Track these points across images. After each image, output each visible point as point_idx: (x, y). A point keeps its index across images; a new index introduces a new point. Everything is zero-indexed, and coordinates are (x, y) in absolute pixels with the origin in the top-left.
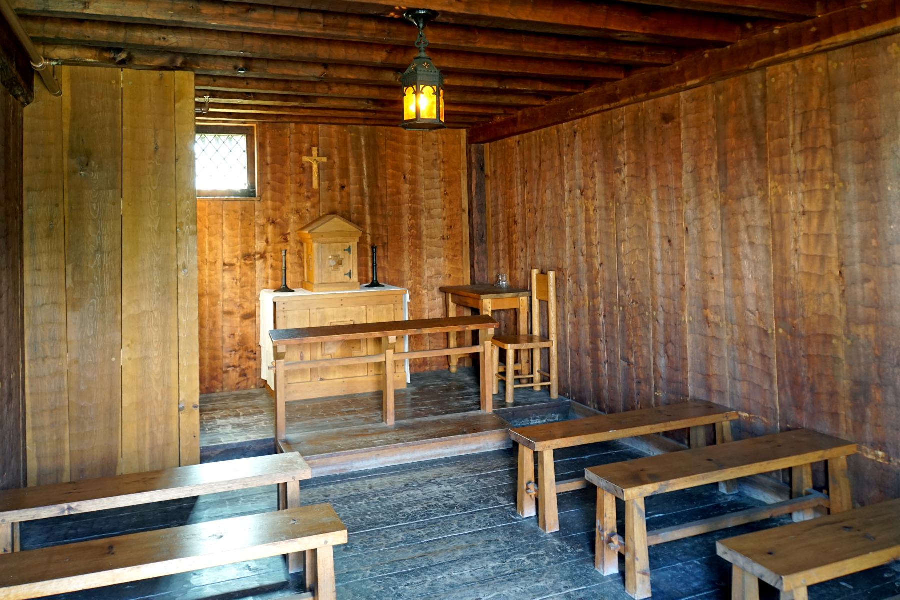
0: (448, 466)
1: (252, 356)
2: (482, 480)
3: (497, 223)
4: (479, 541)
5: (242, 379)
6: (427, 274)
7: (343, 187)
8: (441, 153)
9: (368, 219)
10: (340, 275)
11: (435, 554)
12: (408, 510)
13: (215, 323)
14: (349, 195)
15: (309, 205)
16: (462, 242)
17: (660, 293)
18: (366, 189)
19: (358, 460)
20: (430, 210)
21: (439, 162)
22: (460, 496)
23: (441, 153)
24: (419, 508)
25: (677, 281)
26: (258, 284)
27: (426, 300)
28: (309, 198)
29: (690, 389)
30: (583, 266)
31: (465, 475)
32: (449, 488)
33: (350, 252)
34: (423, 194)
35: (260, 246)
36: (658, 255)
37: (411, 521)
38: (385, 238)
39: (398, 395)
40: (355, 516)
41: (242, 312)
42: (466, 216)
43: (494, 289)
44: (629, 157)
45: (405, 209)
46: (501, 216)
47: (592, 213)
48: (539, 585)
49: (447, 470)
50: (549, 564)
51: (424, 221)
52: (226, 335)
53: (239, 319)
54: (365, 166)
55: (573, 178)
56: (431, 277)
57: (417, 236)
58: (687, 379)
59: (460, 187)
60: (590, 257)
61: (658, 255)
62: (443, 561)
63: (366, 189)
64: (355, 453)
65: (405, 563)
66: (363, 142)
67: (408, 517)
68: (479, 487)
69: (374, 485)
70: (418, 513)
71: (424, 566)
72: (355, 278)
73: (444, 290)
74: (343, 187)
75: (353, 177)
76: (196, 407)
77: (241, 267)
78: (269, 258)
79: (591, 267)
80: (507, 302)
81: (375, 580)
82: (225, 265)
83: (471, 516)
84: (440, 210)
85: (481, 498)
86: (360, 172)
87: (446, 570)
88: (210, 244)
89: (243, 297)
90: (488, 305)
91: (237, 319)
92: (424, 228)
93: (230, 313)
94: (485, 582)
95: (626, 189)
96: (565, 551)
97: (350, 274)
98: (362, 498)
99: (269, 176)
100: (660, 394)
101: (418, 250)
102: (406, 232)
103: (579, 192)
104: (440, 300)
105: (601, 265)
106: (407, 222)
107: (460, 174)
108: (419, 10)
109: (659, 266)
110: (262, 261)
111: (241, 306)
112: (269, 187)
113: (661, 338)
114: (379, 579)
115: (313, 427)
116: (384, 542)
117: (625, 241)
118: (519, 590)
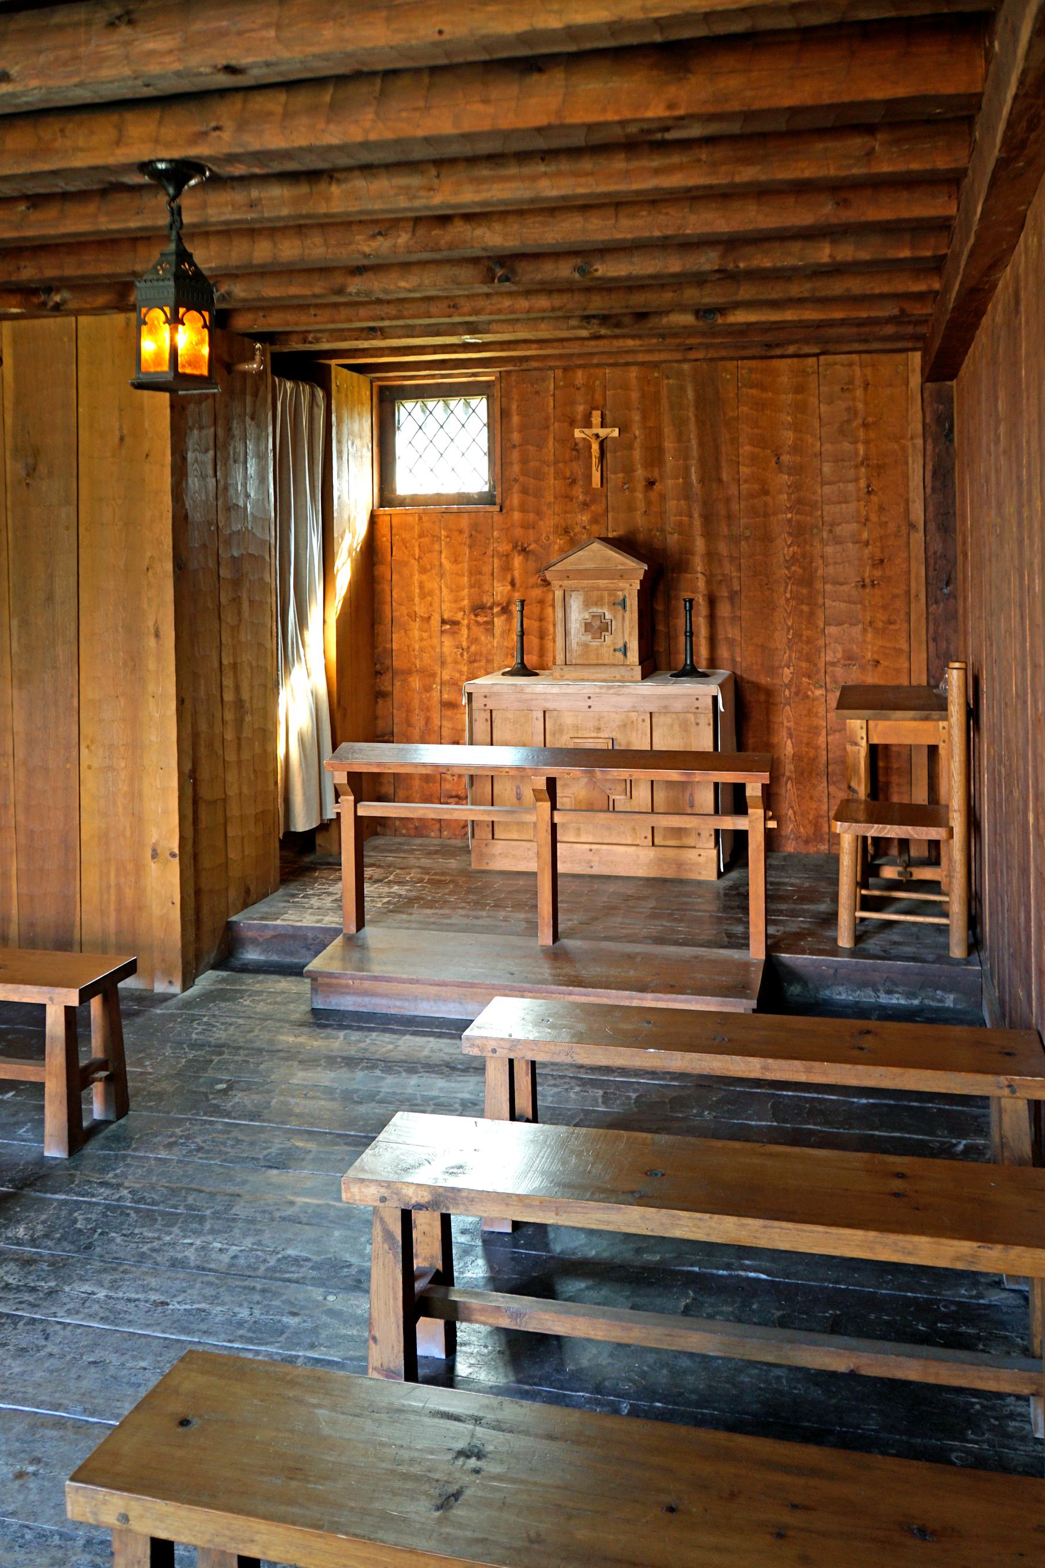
7: (651, 484)
38: (735, 583)
59: (906, 477)
74: (651, 484)
77: (469, 627)
82: (444, 622)
84: (854, 526)
88: (421, 586)
97: (625, 650)
106: (784, 547)
107: (904, 449)
110: (503, 617)
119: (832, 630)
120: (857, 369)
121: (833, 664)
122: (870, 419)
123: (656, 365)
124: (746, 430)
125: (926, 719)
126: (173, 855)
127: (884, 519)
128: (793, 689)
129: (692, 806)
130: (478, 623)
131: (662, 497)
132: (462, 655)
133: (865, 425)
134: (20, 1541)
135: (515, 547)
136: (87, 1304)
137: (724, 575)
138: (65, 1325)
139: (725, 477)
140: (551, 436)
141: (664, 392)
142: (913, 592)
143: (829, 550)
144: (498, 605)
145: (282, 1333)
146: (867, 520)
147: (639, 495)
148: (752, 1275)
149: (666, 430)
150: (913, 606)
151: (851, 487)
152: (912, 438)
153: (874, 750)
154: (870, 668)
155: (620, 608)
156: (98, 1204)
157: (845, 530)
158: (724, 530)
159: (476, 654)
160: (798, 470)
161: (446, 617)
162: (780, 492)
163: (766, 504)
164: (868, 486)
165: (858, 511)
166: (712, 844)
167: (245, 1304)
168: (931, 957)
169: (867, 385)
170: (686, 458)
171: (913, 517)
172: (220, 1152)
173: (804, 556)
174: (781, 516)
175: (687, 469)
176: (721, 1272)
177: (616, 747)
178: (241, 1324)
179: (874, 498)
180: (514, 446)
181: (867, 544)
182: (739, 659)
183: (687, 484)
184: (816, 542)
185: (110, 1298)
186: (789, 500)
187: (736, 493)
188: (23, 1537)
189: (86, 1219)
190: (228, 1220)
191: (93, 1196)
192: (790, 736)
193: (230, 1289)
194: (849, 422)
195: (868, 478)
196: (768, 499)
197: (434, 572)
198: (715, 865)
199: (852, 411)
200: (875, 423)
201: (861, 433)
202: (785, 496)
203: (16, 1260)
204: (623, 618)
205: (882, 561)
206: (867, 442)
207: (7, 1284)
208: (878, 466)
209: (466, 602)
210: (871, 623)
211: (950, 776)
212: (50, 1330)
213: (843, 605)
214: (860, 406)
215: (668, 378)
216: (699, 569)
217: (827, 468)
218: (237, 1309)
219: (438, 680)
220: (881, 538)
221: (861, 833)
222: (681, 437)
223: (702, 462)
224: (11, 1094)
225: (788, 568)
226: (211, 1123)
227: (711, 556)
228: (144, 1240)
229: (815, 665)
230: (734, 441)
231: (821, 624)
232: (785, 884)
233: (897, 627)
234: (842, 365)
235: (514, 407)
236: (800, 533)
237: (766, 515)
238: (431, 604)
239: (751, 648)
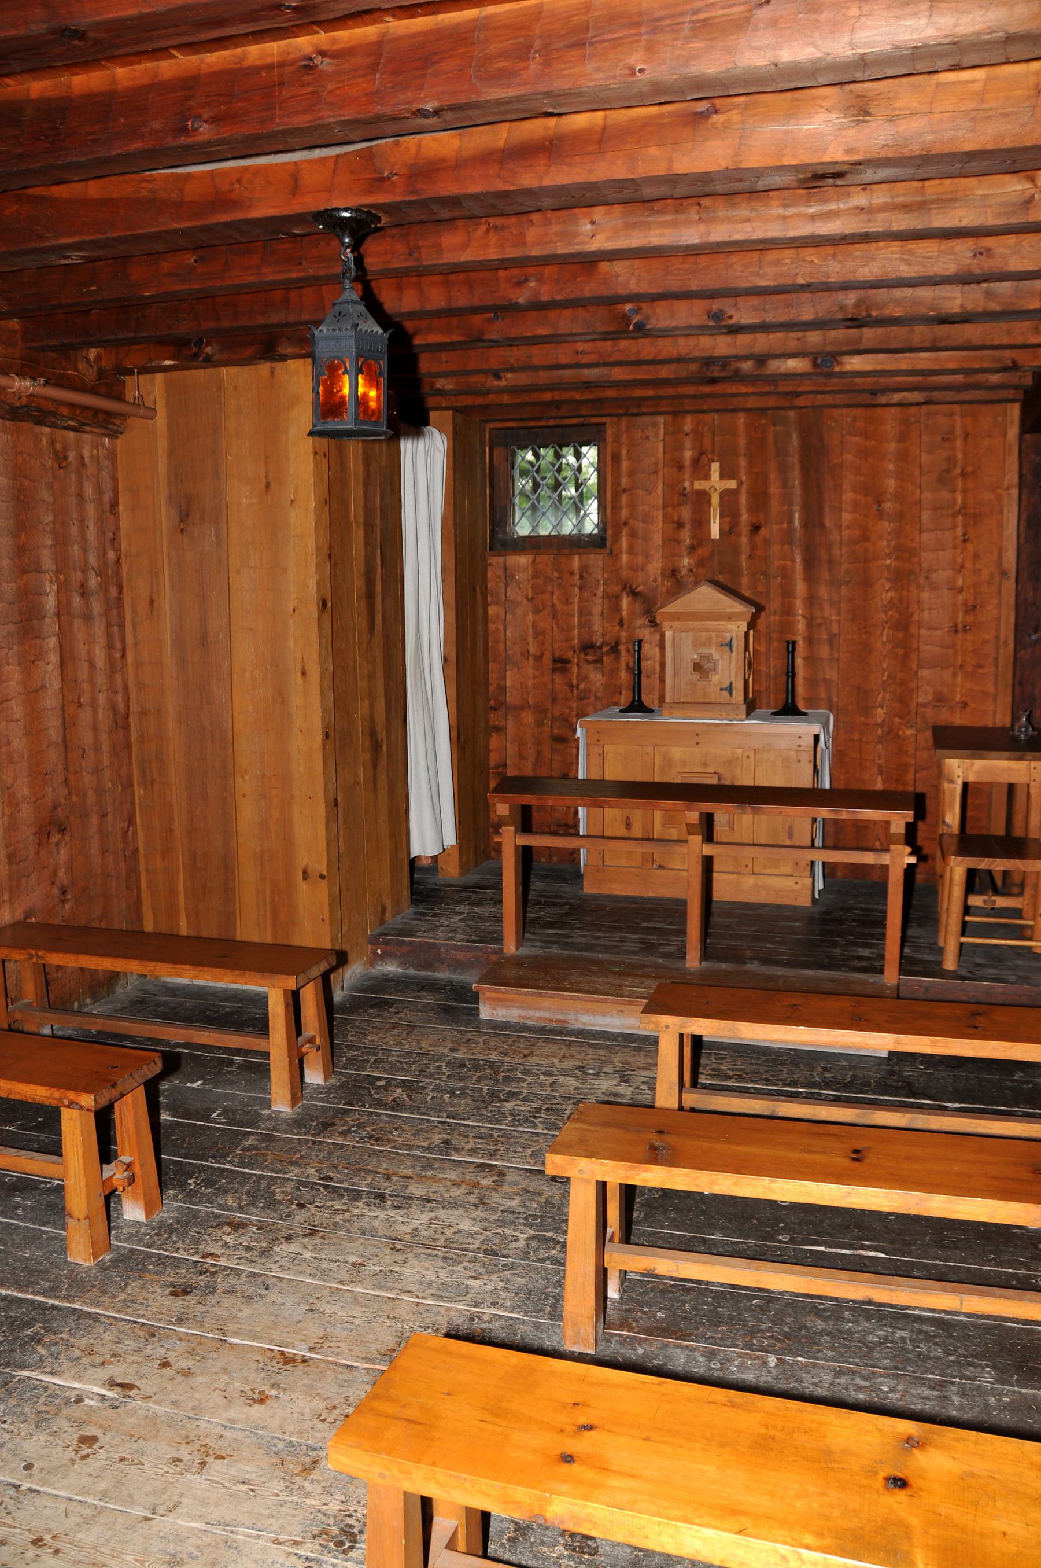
7: (756, 528)
16: (997, 638)
19: (588, 1012)
38: (835, 626)
59: (1001, 526)
64: (579, 998)
74: (756, 528)
78: (623, 653)
82: (555, 661)
84: (949, 573)
86: (787, 500)
106: (884, 593)
107: (999, 498)
108: (338, 210)
110: (613, 656)
119: (925, 673)
120: (958, 419)
121: (924, 705)
122: (969, 469)
123: (763, 410)
124: (849, 480)
125: (1020, 759)
126: (322, 877)
127: (978, 566)
128: (886, 729)
129: (790, 836)
130: (588, 662)
131: (767, 542)
133: (963, 474)
134: (274, 1449)
135: (624, 589)
136: (296, 1262)
137: (823, 618)
138: (281, 1279)
139: (828, 522)
140: (661, 481)
141: (771, 437)
142: (1002, 638)
143: (925, 595)
144: (608, 644)
145: (467, 1293)
146: (962, 567)
147: (744, 540)
148: (872, 1254)
149: (772, 476)
150: (1001, 651)
151: (948, 534)
152: (1008, 489)
153: (965, 785)
154: (958, 710)
155: (727, 649)
156: (291, 1180)
157: (942, 576)
158: (826, 575)
159: (585, 691)
160: (900, 517)
162: (880, 538)
163: (866, 550)
164: (965, 535)
165: (954, 558)
166: (808, 873)
167: (431, 1268)
168: (1012, 978)
169: (966, 435)
170: (791, 504)
171: (1005, 565)
172: (388, 1140)
173: (901, 601)
174: (880, 562)
175: (791, 515)
176: (844, 1251)
177: (723, 782)
178: (430, 1285)
179: (970, 546)
181: (961, 590)
182: (835, 699)
183: (790, 529)
184: (913, 588)
185: (316, 1258)
186: (888, 546)
187: (838, 537)
188: (275, 1446)
189: (283, 1192)
190: (405, 1198)
191: (285, 1173)
192: (881, 773)
193: (417, 1256)
194: (948, 471)
195: (964, 526)
196: (869, 545)
197: (546, 612)
198: (809, 892)
199: (951, 461)
200: (974, 473)
201: (960, 483)
202: (885, 543)
203: (229, 1224)
204: (730, 658)
205: (974, 607)
206: (964, 491)
207: (226, 1243)
208: (975, 515)
210: (961, 666)
212: (268, 1282)
213: (936, 649)
214: (959, 455)
215: (774, 425)
216: (800, 612)
217: (926, 516)
218: (424, 1272)
219: (549, 715)
220: (975, 584)
221: (972, 866)
222: (785, 484)
223: (806, 508)
224: (200, 1082)
225: (885, 612)
226: (378, 1115)
227: (811, 600)
228: (336, 1212)
229: (907, 706)
230: (838, 487)
231: (914, 666)
232: (875, 910)
233: (984, 671)
234: (944, 415)
235: (624, 452)
236: (901, 578)
237: (866, 561)
238: (543, 644)
239: (847, 689)
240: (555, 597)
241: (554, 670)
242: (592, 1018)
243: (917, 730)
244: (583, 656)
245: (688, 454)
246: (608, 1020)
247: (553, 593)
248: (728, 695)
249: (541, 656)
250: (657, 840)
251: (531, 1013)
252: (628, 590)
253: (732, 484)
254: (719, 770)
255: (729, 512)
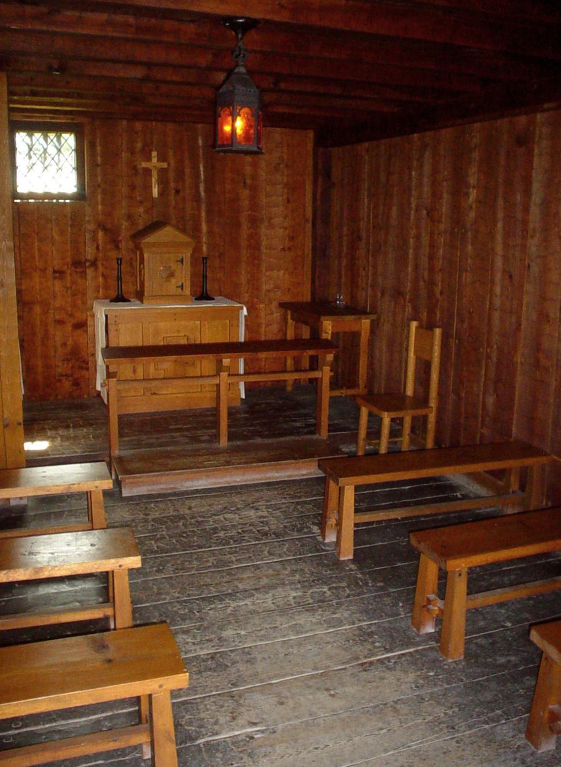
0: (268, 490)
1: (85, 366)
2: (299, 507)
3: (341, 237)
4: (286, 569)
5: (75, 388)
6: (265, 287)
8: (285, 157)
9: (204, 227)
10: (172, 286)
11: (241, 580)
12: (222, 534)
13: (46, 331)
14: (184, 199)
15: (141, 210)
17: (496, 330)
18: (203, 194)
19: (188, 479)
20: (270, 218)
21: (282, 166)
22: (274, 524)
23: (285, 157)
24: (234, 533)
25: (514, 319)
26: (90, 293)
27: (263, 314)
28: (141, 202)
29: (514, 429)
30: (423, 293)
31: (284, 501)
32: (265, 514)
33: (182, 263)
34: (263, 200)
35: (89, 252)
36: (498, 290)
37: (224, 545)
39: (231, 414)
40: (171, 537)
41: (75, 321)
42: (309, 226)
43: (331, 310)
44: (478, 180)
45: (243, 219)
46: (345, 229)
47: (436, 237)
48: (335, 616)
49: (267, 494)
50: (348, 596)
51: (263, 230)
52: (59, 343)
53: (70, 329)
54: (202, 169)
55: (420, 197)
56: (269, 291)
57: (255, 246)
58: (512, 419)
60: (431, 283)
61: (498, 290)
62: (247, 587)
63: (203, 194)
65: (211, 588)
66: (200, 142)
67: (224, 542)
68: (296, 514)
69: (193, 505)
70: (232, 537)
71: (230, 591)
72: (187, 291)
73: (283, 305)
75: (188, 180)
76: (19, 424)
77: (71, 275)
78: (100, 266)
79: (431, 295)
80: (349, 323)
81: (180, 603)
82: (55, 272)
83: (282, 544)
85: (295, 526)
87: (250, 597)
88: (39, 250)
89: (74, 305)
90: (328, 327)
91: (69, 327)
92: (263, 238)
93: (61, 322)
94: (284, 610)
95: (472, 215)
96: (366, 584)
97: (182, 287)
98: (180, 519)
99: (99, 179)
100: (485, 431)
101: (256, 262)
102: (244, 243)
103: (425, 212)
104: (277, 315)
105: (441, 293)
106: (245, 231)
109: (497, 302)
110: (93, 269)
111: (72, 315)
112: (99, 191)
113: (492, 374)
114: (185, 601)
115: (139, 444)
116: (195, 564)
117: (466, 271)
118: (314, 620)
132: (67, 291)
135: (99, 225)
161: (56, 269)
180: (98, 165)
209: (69, 260)
211: (242, 331)
240: (54, 232)
241: (55, 278)
242: (191, 483)
243: (266, 305)
244: (73, 268)
245: (139, 145)
246: (200, 482)
247: (52, 229)
248: (180, 290)
249: (45, 269)
250: (152, 379)
251: (155, 487)
252: (102, 227)
253: (165, 165)
254: (187, 334)
255: (163, 182)
